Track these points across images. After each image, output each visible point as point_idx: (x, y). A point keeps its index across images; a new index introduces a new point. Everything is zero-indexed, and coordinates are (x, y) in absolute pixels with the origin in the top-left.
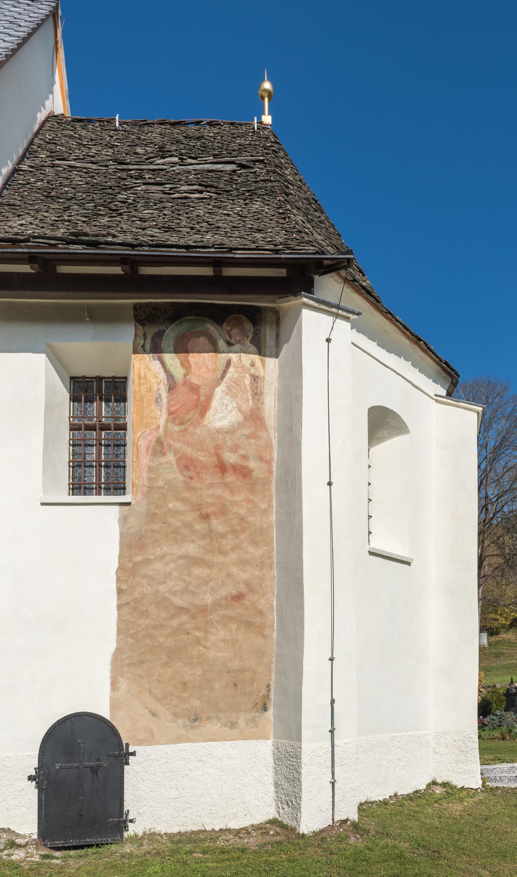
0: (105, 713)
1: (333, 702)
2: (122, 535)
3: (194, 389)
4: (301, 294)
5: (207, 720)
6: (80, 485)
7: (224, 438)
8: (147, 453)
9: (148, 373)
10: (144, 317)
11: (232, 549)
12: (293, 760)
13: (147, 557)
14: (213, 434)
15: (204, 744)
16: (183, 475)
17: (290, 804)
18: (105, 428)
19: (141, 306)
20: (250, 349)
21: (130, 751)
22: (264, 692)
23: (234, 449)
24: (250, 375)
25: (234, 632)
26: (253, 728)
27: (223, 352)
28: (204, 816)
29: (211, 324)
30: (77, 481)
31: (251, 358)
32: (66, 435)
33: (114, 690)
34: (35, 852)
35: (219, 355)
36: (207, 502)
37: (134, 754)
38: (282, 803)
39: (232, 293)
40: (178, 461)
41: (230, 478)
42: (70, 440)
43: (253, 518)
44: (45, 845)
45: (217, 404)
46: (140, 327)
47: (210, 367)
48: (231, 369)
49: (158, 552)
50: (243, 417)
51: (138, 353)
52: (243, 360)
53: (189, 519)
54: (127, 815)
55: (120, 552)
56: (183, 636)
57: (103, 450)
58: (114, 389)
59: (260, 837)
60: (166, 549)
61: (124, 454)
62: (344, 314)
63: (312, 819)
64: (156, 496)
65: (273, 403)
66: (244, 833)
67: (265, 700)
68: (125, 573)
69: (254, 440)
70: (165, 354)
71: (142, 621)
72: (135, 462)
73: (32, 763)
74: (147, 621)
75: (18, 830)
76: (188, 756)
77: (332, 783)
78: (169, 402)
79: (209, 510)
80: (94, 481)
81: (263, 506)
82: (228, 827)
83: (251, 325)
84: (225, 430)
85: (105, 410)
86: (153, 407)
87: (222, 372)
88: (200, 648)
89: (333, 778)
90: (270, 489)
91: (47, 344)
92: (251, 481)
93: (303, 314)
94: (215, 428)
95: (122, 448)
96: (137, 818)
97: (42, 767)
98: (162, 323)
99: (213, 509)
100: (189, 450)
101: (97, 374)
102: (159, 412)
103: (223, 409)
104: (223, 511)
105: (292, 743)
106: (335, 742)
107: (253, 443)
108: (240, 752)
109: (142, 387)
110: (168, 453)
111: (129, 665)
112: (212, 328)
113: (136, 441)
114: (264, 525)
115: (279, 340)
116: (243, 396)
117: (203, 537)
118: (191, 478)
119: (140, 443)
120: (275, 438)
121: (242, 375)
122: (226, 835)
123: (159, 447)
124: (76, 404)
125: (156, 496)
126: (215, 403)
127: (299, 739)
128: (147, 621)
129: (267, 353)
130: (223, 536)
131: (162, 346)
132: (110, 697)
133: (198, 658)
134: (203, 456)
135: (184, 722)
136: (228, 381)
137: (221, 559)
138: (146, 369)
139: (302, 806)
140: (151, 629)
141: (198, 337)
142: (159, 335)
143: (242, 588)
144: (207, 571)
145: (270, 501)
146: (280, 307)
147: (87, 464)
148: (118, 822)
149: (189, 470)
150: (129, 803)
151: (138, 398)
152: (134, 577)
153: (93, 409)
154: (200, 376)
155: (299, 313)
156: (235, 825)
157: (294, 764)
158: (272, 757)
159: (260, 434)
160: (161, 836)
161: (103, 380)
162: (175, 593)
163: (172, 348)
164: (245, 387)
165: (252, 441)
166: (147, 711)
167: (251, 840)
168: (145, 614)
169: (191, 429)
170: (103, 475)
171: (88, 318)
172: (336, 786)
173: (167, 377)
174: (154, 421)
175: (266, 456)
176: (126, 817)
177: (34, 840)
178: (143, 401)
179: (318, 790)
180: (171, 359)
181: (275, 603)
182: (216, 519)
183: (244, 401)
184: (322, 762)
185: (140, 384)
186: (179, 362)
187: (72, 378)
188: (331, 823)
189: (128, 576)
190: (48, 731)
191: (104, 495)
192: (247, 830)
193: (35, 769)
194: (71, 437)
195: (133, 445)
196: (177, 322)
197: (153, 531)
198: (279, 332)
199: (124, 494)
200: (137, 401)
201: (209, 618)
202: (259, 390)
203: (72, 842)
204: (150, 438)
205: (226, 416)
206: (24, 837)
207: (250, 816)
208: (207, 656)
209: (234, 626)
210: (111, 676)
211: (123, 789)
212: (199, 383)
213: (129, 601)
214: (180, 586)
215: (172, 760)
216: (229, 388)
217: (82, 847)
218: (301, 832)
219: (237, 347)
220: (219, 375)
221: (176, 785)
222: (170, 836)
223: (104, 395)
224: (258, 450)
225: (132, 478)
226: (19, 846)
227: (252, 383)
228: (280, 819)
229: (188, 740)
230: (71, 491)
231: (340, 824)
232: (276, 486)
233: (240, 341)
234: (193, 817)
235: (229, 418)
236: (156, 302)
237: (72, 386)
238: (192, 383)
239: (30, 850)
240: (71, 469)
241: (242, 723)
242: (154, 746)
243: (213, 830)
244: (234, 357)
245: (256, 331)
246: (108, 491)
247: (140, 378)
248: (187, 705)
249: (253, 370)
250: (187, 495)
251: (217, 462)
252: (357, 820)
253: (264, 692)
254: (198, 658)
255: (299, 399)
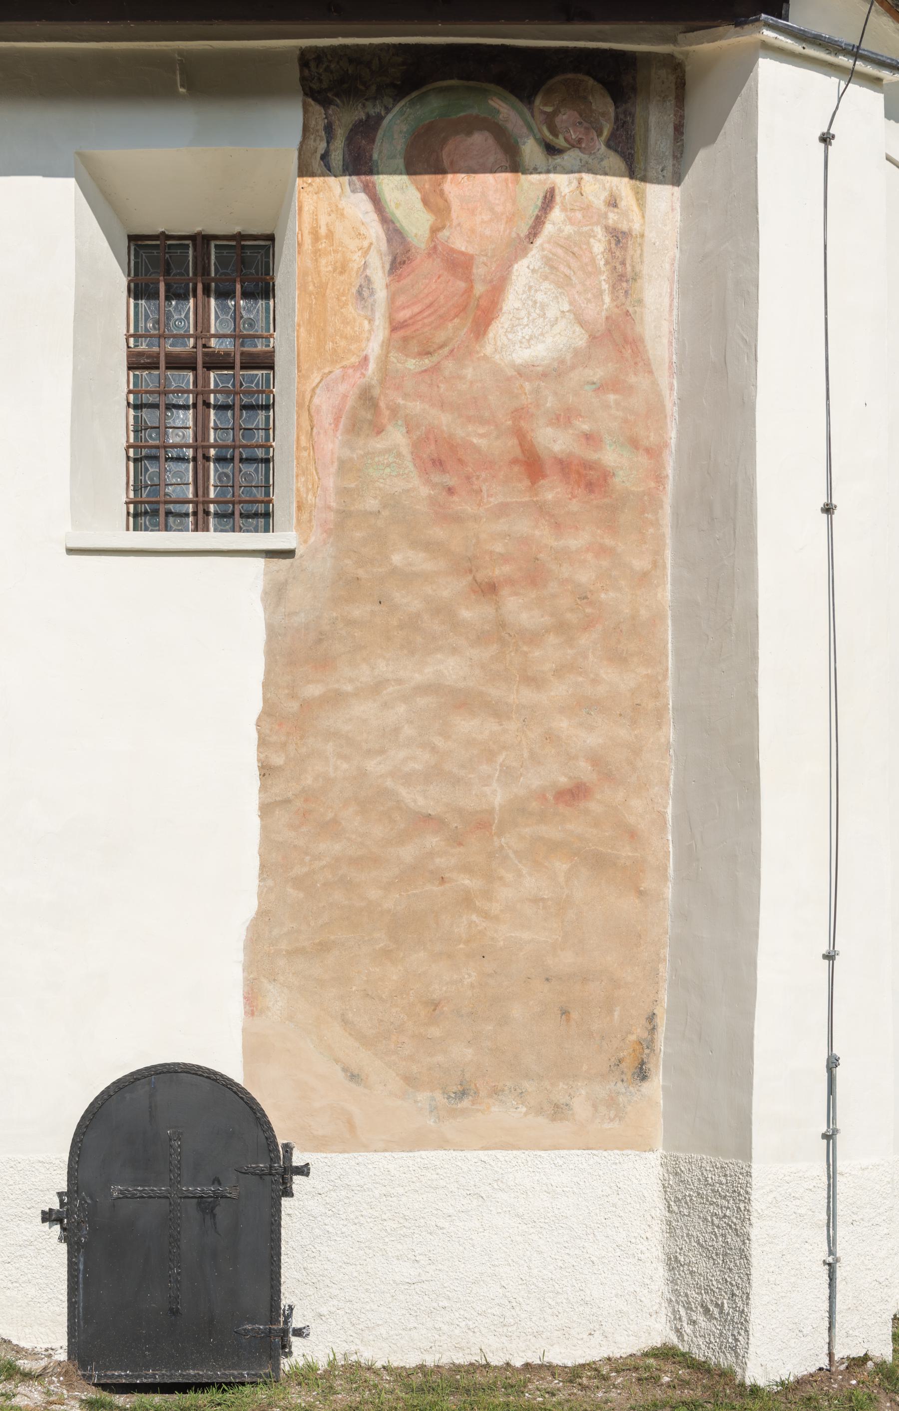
0: (232, 1067)
1: (832, 1064)
2: (272, 633)
3: (459, 265)
4: (758, 20)
5: (490, 1096)
6: (155, 506)
7: (537, 391)
8: (337, 426)
9: (340, 228)
10: (327, 83)
11: (556, 671)
12: (725, 1203)
13: (336, 686)
14: (509, 379)
15: (482, 1154)
16: (428, 482)
17: (716, 1311)
18: (218, 362)
19: (319, 55)
20: (605, 163)
21: (294, 1164)
22: (639, 1032)
23: (563, 418)
24: (607, 228)
25: (561, 879)
26: (611, 1120)
27: (535, 171)
28: (484, 1331)
29: (504, 100)
30: (148, 496)
31: (607, 185)
32: (119, 379)
33: (253, 1014)
34: (65, 1392)
35: (523, 177)
36: (491, 553)
37: (304, 1171)
38: (689, 1308)
39: (569, 19)
40: (416, 446)
41: (552, 491)
42: (130, 392)
43: (612, 594)
44: (87, 1378)
45: (518, 304)
46: (317, 110)
47: (499, 209)
48: (556, 214)
49: (365, 674)
50: (586, 336)
51: (313, 175)
52: (587, 193)
53: (446, 593)
54: (288, 1317)
55: (268, 672)
56: (429, 887)
57: (212, 417)
58: (244, 264)
59: (636, 1388)
60: (383, 668)
61: (267, 430)
62: (869, 69)
63: (775, 1355)
64: (358, 535)
65: (667, 301)
66: (590, 1378)
67: (642, 1054)
68: (280, 724)
69: (617, 397)
70: (381, 177)
71: (322, 847)
72: (305, 449)
73: (52, 1180)
74: (337, 847)
75: (19, 1339)
76: (443, 1183)
77: (829, 1264)
78: (392, 299)
79: (497, 572)
80: (191, 496)
81: (640, 564)
82: (546, 1359)
83: (609, 100)
84: (540, 369)
85: (217, 317)
86: (352, 310)
87: (531, 222)
88: (474, 917)
89: (831, 1252)
90: (657, 520)
91: (79, 154)
92: (607, 500)
93: (760, 70)
94: (513, 365)
95: (262, 414)
96: (312, 1326)
97: (77, 1192)
98: (375, 98)
99: (507, 569)
100: (445, 420)
101: (198, 229)
102: (366, 322)
103: (534, 315)
104: (534, 576)
105: (720, 1161)
106: (838, 1163)
107: (612, 403)
108: (575, 1179)
109: (323, 261)
110: (390, 428)
111: (294, 953)
112: (505, 109)
113: (308, 396)
114: (643, 612)
115: (684, 137)
116: (588, 283)
117: (481, 639)
118: (450, 491)
119: (316, 401)
120: (671, 389)
121: (585, 229)
122: (543, 1379)
123: (367, 412)
124: (142, 302)
125: (358, 535)
126: (512, 301)
127: (745, 1151)
128: (337, 847)
129: (652, 173)
130: (534, 638)
131: (375, 156)
132: (244, 1030)
133: (467, 942)
134: (482, 436)
135: (433, 1099)
136: (546, 246)
137: (527, 695)
138: (333, 216)
139: (752, 1318)
140: (344, 867)
141: (469, 133)
142: (366, 129)
143: (584, 770)
144: (492, 726)
145: (658, 552)
146: (687, 54)
147: (173, 453)
148: (272, 1335)
149: (444, 471)
150: (293, 1290)
151: (311, 288)
152: (302, 738)
153: (187, 316)
154: (473, 231)
155: (747, 69)
156: (565, 1355)
157: (728, 1213)
158: (662, 1195)
159: (632, 379)
160: (376, 1372)
161: (213, 244)
162: (408, 779)
163: (400, 162)
164: (593, 260)
165: (612, 397)
166: (338, 1068)
167: (613, 1394)
168: (331, 828)
169: (449, 366)
170: (212, 482)
171: (182, 86)
172: (840, 1274)
173: (386, 234)
174: (353, 347)
175: (648, 437)
176: (286, 1322)
177: (60, 1363)
178: (324, 296)
179: (793, 1279)
180: (398, 189)
181: (669, 810)
182: (516, 594)
183: (589, 296)
184: (802, 1211)
185: (317, 253)
186: (419, 195)
187: (132, 238)
188: (824, 1362)
189: (288, 734)
190: (91, 1104)
191: (215, 530)
192: (596, 1370)
193: (60, 1195)
194: (131, 387)
195: (300, 405)
196: (414, 94)
197: (350, 623)
198: (682, 117)
199: (267, 530)
200: (310, 294)
201: (496, 842)
202: (629, 268)
203: (154, 1376)
204: (342, 388)
205: (542, 334)
206: (33, 1354)
207: (601, 1338)
208: (493, 939)
209: (561, 866)
210: (246, 979)
211: (279, 1254)
212: (470, 251)
213: (290, 794)
214: (421, 760)
215: (401, 1190)
216: (549, 262)
217: (183, 1388)
218: (748, 1382)
219: (571, 157)
220: (524, 229)
221: (413, 1250)
222: (401, 1375)
223: (213, 280)
224: (626, 421)
225: (298, 490)
226: (27, 1376)
227: (610, 250)
228: (684, 1348)
229: (443, 1144)
230: (131, 519)
231: (847, 1368)
232: (676, 514)
233: (580, 141)
234: (457, 1332)
235: (549, 340)
236: (358, 45)
237: (132, 257)
238: (452, 250)
239: (52, 1387)
240: (131, 464)
241: (580, 1107)
242: (356, 1155)
243: (508, 1364)
244: (563, 182)
245: (621, 116)
246: (228, 519)
247: (316, 238)
248: (440, 1058)
249: (613, 217)
250: (438, 533)
251: (518, 452)
252: (889, 1358)
253: (639, 1032)
254: (467, 942)
255: (748, 292)
